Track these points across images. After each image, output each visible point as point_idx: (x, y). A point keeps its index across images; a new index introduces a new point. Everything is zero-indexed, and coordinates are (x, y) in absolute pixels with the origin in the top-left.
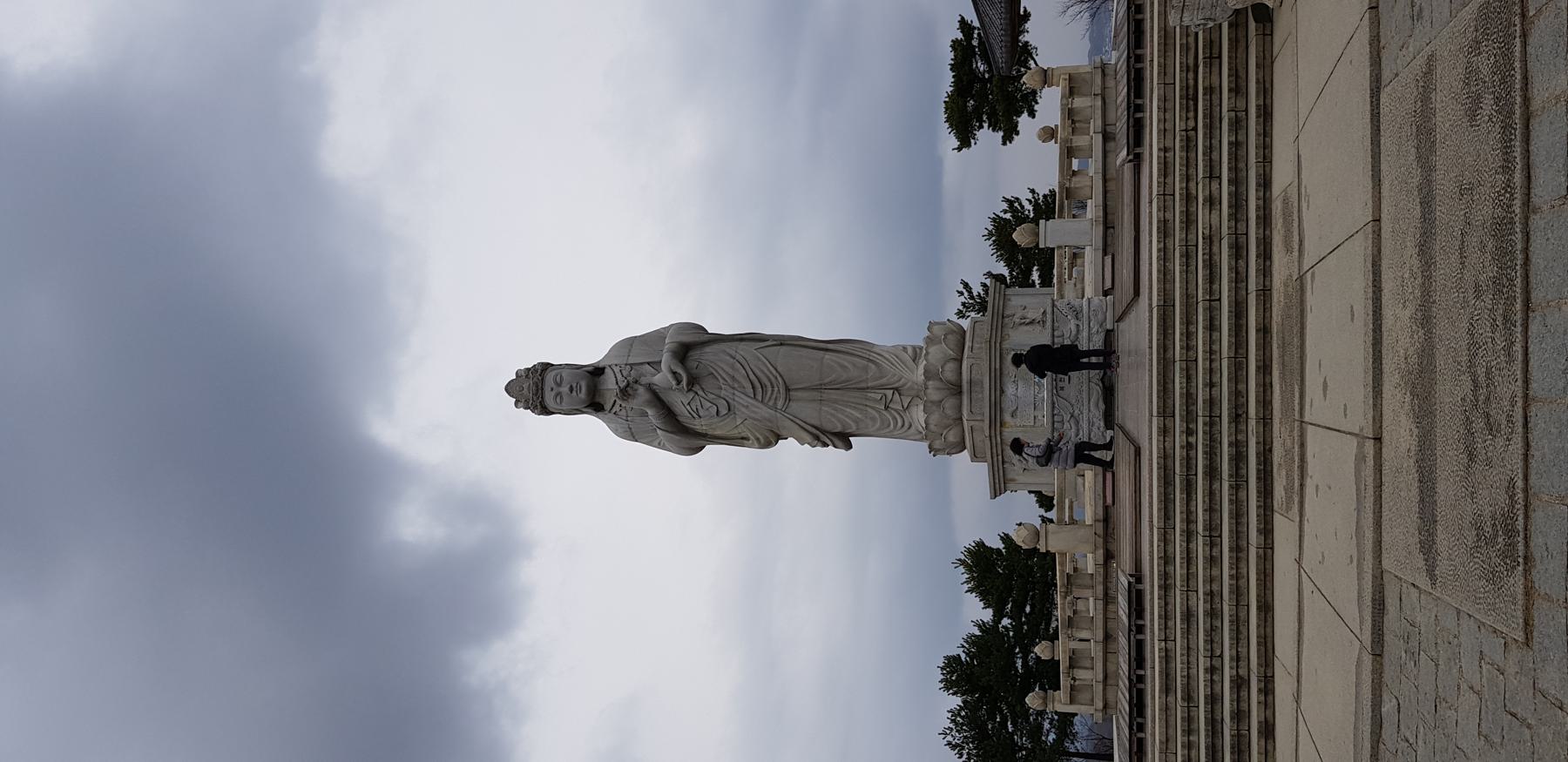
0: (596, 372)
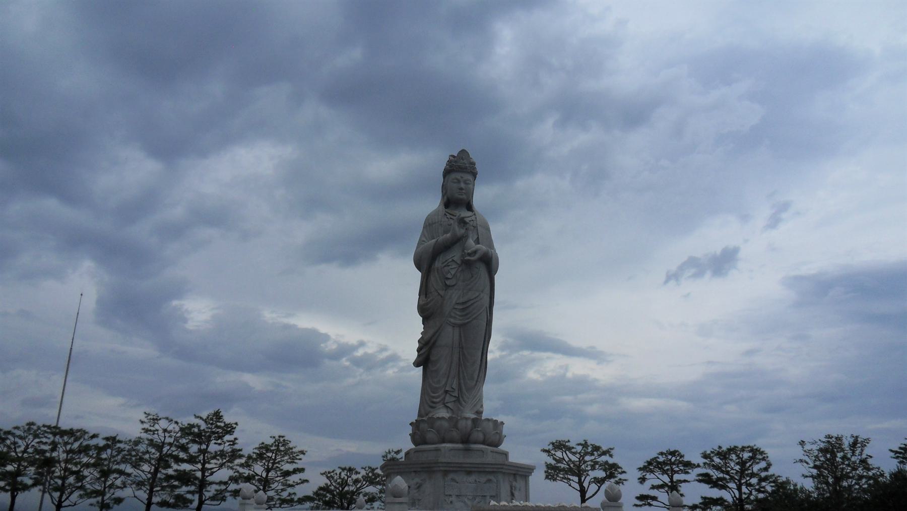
0: (469, 207)
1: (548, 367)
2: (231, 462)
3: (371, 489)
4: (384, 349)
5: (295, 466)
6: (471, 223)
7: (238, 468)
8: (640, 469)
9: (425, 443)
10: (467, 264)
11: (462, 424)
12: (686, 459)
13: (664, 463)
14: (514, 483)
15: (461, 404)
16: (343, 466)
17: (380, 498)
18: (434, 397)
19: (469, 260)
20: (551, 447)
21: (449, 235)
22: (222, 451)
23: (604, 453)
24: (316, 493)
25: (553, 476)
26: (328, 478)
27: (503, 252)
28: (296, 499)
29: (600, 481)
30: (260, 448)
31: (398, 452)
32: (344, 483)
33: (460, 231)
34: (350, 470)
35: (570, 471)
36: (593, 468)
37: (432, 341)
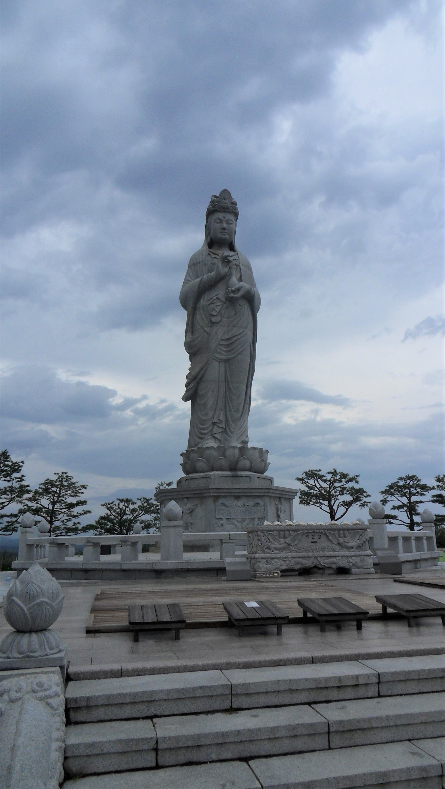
0: (232, 248)
1: (296, 414)
2: (20, 497)
3: (147, 517)
4: (162, 401)
5: (78, 499)
6: (234, 262)
7: (27, 502)
8: (382, 493)
9: (196, 471)
10: (231, 301)
11: (229, 452)
12: (422, 483)
13: (404, 487)
14: (279, 506)
15: (228, 436)
16: (121, 498)
17: (155, 525)
19: (232, 298)
21: (213, 273)
22: (11, 487)
23: (351, 480)
24: (97, 522)
25: (306, 501)
26: (108, 508)
27: (265, 296)
28: (80, 527)
29: (348, 505)
30: (45, 484)
31: (169, 484)
32: (122, 513)
33: (224, 270)
34: (127, 501)
35: (321, 496)
36: (341, 493)
37: (199, 377)
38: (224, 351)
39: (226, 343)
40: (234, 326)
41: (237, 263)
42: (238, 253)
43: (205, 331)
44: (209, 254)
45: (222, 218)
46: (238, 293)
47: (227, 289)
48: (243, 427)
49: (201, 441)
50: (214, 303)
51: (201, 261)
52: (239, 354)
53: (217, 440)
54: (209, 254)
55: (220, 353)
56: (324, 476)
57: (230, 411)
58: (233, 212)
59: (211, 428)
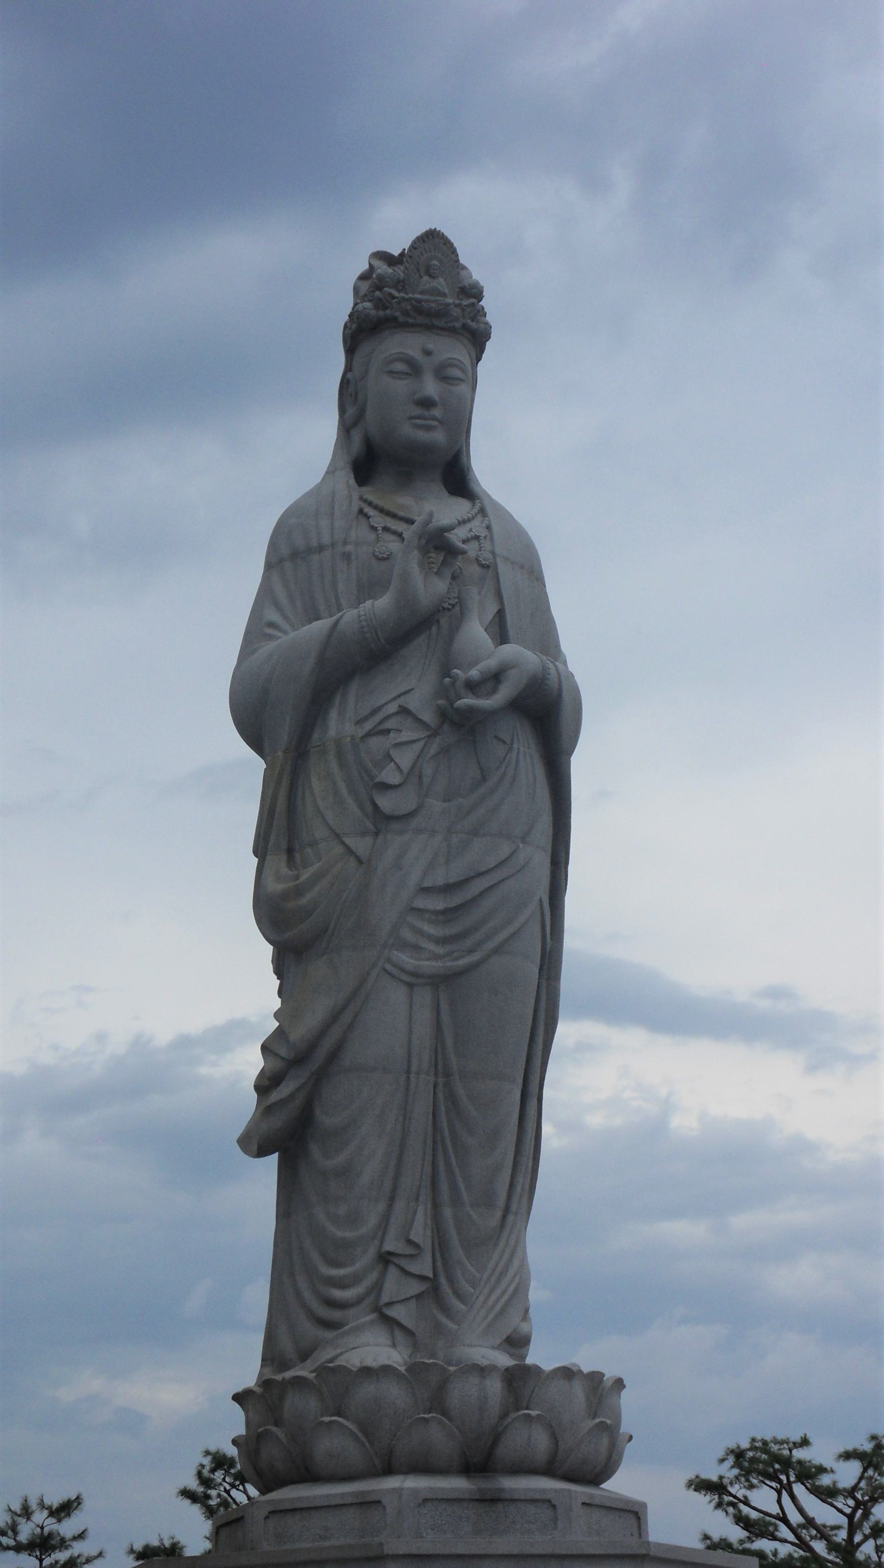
0: (457, 479)
6: (471, 549)
10: (461, 726)
11: (463, 1393)
15: (445, 1309)
18: (341, 1284)
19: (471, 710)
20: (728, 1471)
33: (430, 588)
38: (430, 938)
39: (438, 904)
40: (475, 833)
41: (485, 556)
42: (489, 509)
43: (350, 851)
44: (361, 511)
45: (416, 354)
46: (494, 690)
47: (445, 671)
48: (511, 1272)
49: (329, 1335)
50: (388, 731)
51: (326, 540)
52: (496, 951)
53: (399, 1335)
54: (361, 511)
55: (416, 948)
56: (821, 1470)
57: (456, 1201)
58: (465, 327)
59: (374, 1276)
